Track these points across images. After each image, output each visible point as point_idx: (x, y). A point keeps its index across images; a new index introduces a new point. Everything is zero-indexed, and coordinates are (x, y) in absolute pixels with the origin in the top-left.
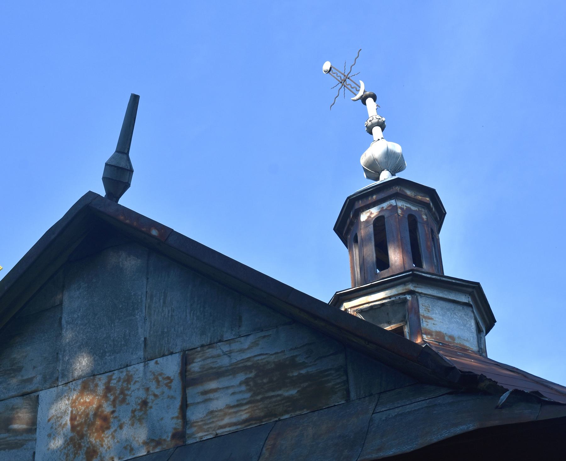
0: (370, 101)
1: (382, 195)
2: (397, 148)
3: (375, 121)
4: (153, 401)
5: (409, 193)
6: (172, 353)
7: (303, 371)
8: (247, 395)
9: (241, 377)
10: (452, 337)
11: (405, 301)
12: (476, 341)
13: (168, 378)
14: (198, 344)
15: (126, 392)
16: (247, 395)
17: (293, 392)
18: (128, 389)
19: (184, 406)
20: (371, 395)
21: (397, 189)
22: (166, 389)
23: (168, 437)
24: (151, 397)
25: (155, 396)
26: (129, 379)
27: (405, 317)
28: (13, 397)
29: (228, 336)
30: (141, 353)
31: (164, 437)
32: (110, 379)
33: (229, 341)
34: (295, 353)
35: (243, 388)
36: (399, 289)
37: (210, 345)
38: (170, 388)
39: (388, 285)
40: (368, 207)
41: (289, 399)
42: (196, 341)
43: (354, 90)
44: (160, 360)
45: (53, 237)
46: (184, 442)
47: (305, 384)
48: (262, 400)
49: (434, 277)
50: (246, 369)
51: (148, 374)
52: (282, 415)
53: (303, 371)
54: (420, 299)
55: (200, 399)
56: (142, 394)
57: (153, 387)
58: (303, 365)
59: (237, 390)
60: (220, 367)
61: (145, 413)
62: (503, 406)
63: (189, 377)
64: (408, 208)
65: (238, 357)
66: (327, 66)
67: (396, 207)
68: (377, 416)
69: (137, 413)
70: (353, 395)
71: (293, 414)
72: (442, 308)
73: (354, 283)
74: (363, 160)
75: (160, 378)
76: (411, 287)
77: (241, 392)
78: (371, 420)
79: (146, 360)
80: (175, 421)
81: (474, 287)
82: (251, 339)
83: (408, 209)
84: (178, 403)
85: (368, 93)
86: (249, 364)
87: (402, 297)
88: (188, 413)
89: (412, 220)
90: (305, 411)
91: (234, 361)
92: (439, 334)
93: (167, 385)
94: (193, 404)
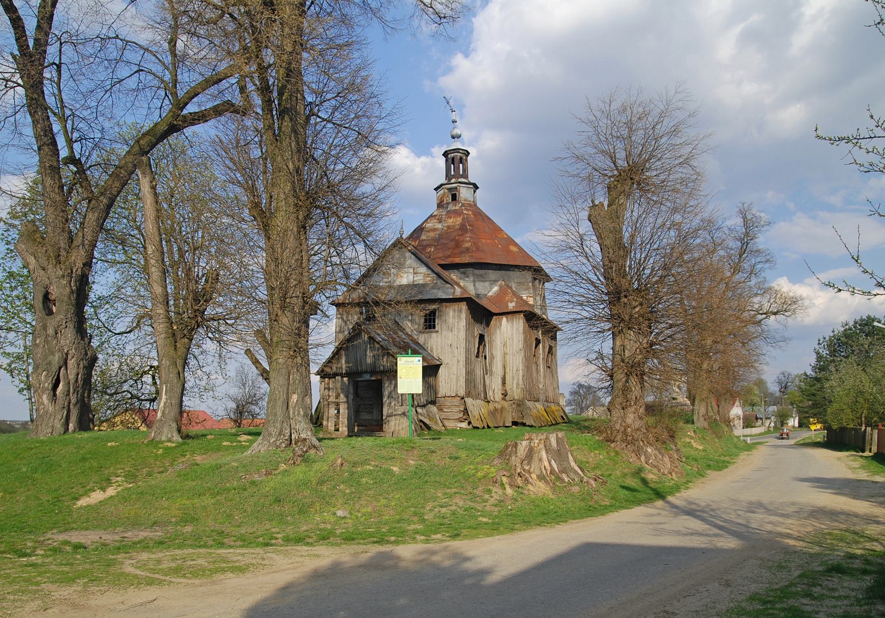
1: (454, 151)
5: (461, 151)
76: (459, 184)
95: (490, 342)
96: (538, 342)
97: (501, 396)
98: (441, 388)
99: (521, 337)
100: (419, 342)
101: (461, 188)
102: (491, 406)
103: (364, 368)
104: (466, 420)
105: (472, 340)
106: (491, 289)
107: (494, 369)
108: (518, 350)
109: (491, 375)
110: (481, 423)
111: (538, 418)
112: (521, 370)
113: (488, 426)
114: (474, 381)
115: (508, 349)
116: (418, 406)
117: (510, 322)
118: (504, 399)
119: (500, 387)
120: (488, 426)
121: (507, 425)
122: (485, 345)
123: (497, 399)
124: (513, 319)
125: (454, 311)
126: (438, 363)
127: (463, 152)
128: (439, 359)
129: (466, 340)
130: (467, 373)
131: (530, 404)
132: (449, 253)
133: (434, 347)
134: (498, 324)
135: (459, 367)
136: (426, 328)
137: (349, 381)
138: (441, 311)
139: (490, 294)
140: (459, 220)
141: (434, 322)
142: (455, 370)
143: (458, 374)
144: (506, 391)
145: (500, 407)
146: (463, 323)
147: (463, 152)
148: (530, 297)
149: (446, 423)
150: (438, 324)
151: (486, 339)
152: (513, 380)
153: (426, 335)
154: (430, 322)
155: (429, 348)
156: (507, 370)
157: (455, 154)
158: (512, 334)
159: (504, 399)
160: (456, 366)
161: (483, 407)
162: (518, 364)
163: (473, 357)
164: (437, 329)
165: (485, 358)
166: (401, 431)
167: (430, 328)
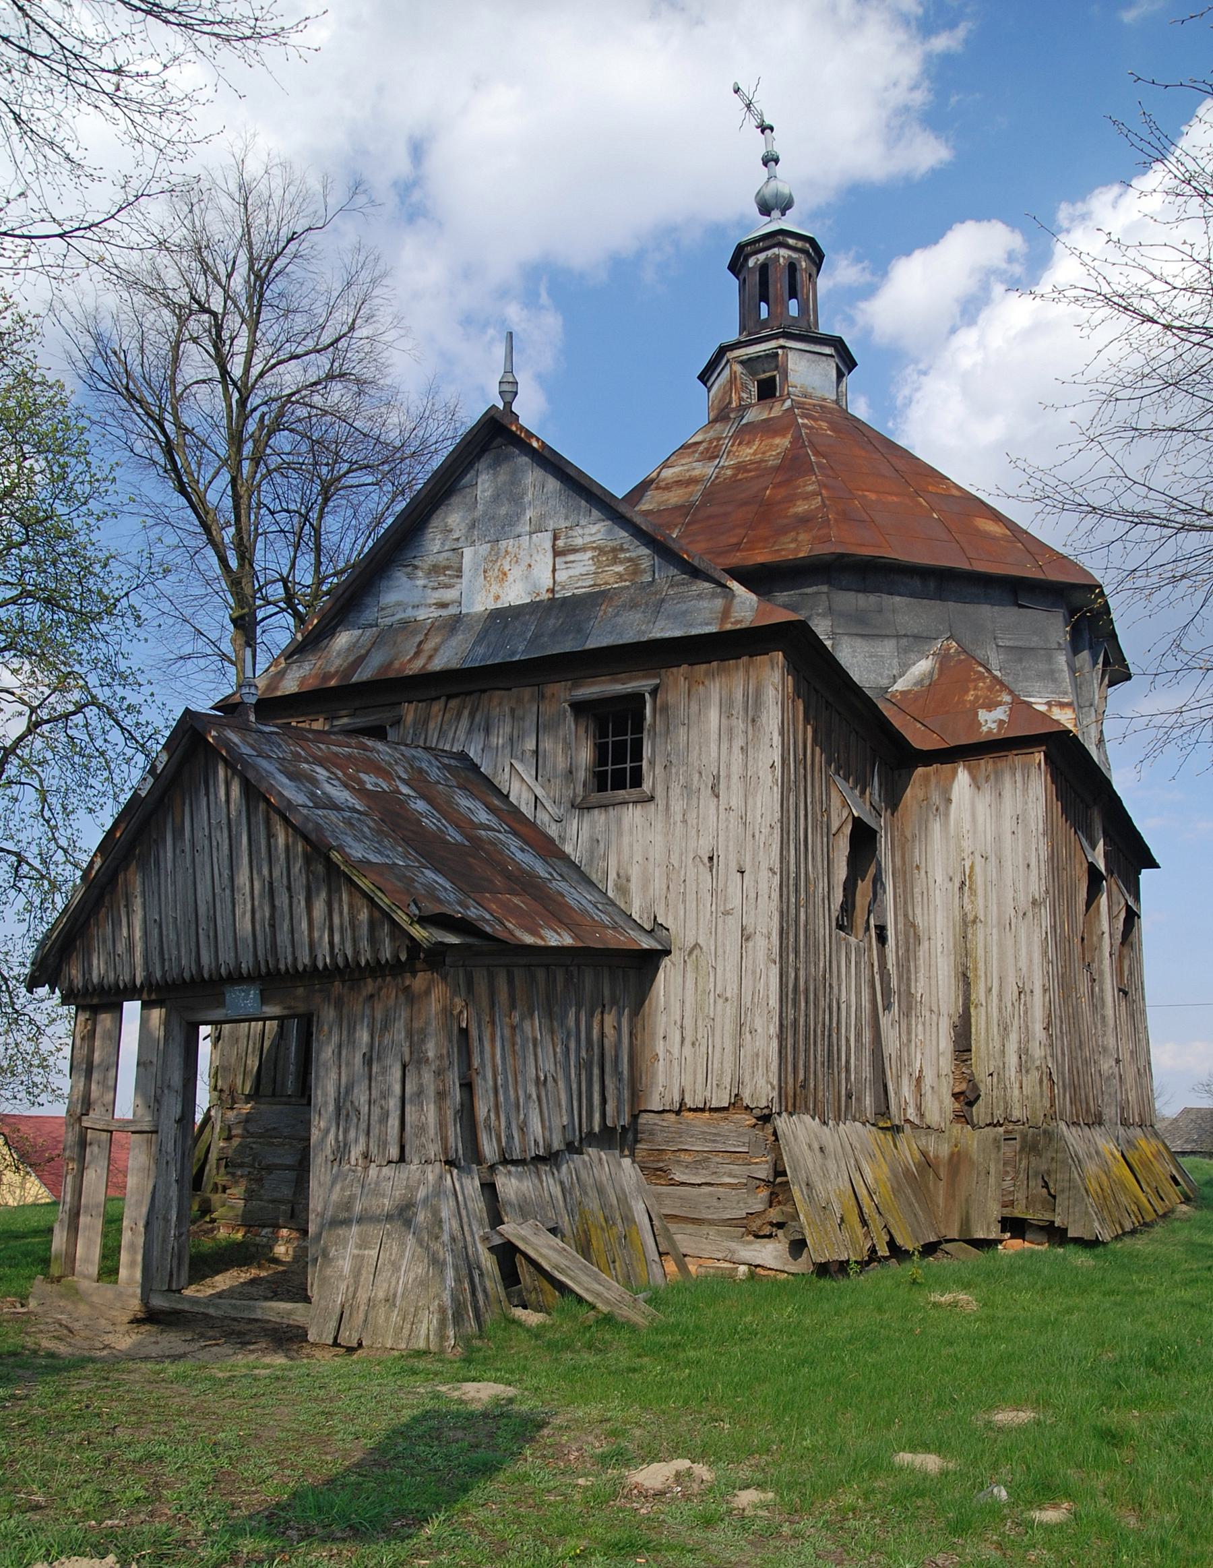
1: (768, 243)
5: (791, 241)
8: (593, 568)
9: (589, 554)
11: (777, 354)
19: (554, 570)
30: (527, 528)
33: (583, 527)
41: (617, 573)
42: (563, 524)
50: (594, 549)
55: (564, 566)
58: (628, 550)
65: (588, 539)
76: (782, 342)
83: (790, 257)
89: (792, 267)
95: (905, 877)
96: (1095, 878)
97: (949, 1104)
98: (661, 1066)
99: (1039, 849)
100: (568, 849)
101: (791, 355)
102: (908, 1150)
103: (226, 957)
104: (780, 1225)
105: (817, 842)
106: (904, 668)
107: (920, 988)
108: (1024, 902)
109: (907, 1012)
110: (860, 1231)
111: (1107, 1202)
112: (1038, 991)
113: (892, 1244)
114: (830, 1033)
115: (980, 901)
116: (505, 1162)
117: (986, 787)
118: (962, 1117)
119: (946, 1063)
120: (892, 1244)
121: (980, 1235)
122: (877, 880)
123: (934, 1116)
124: (998, 775)
125: (726, 709)
126: (646, 943)
127: (800, 244)
128: (657, 928)
129: (784, 832)
130: (790, 993)
131: (1072, 1136)
132: (734, 540)
133: (635, 873)
134: (936, 798)
135: (748, 963)
136: (602, 788)
137: (167, 1023)
138: (665, 708)
139: (900, 686)
140: (783, 442)
141: (638, 755)
142: (732, 976)
143: (747, 999)
144: (971, 1081)
145: (945, 1150)
146: (770, 752)
147: (800, 244)
148: (1062, 705)
149: (685, 1240)
150: (652, 763)
151: (883, 844)
152: (1005, 1029)
153: (599, 817)
154: (619, 758)
155: (612, 876)
156: (979, 993)
157: (770, 253)
158: (998, 839)
159: (962, 1117)
160: (734, 959)
161: (872, 1156)
162: (1023, 963)
163: (823, 927)
164: (646, 786)
165: (882, 938)
166: (382, 1311)
167: (619, 785)
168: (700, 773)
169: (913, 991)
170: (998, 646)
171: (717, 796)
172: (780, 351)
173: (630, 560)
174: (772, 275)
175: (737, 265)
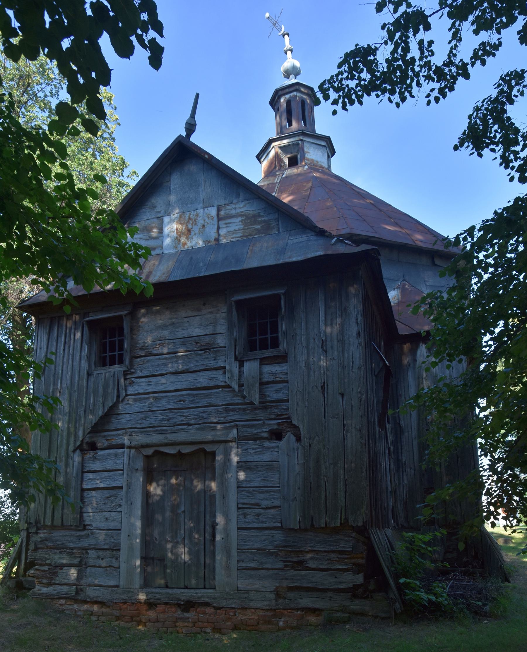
0: (286, 36)
2: (297, 64)
3: (288, 48)
4: (207, 225)
6: (213, 206)
7: (263, 219)
8: (242, 226)
9: (240, 219)
10: (317, 162)
11: (298, 144)
12: (327, 163)
13: (212, 216)
14: (223, 203)
15: (197, 221)
16: (242, 226)
17: (259, 227)
18: (197, 219)
19: (218, 228)
20: (287, 231)
21: (297, 87)
22: (211, 221)
23: (213, 240)
24: (206, 224)
25: (207, 223)
26: (197, 215)
27: (298, 151)
28: (154, 218)
29: (235, 201)
30: (202, 205)
31: (211, 240)
32: (190, 214)
34: (260, 211)
35: (241, 223)
36: (297, 138)
37: (228, 204)
38: (213, 220)
39: (291, 136)
40: (284, 94)
41: (257, 229)
42: (223, 202)
43: (279, 30)
44: (209, 208)
45: (167, 153)
46: (219, 242)
47: (263, 224)
48: (248, 229)
49: (311, 133)
50: (242, 216)
51: (205, 214)
52: (255, 235)
53: (263, 219)
54: (305, 144)
55: (225, 226)
56: (202, 222)
57: (207, 219)
58: (263, 216)
59: (238, 224)
60: (232, 214)
61: (204, 230)
62: (333, 244)
63: (220, 217)
64: (301, 97)
65: (238, 211)
66: (267, 15)
67: (296, 96)
68: (289, 241)
69: (201, 230)
70: (281, 230)
71: (259, 235)
72: (314, 148)
73: (277, 134)
74: (282, 69)
75: (209, 216)
76: (301, 138)
77: (240, 225)
78: (287, 243)
79: (204, 208)
80: (215, 234)
81: (327, 138)
82: (243, 204)
84: (216, 227)
85: (285, 32)
86: (242, 214)
87: (297, 142)
88: (220, 231)
89: (303, 102)
90: (263, 235)
91: (237, 212)
92: (312, 160)
93: (212, 219)
94: (222, 228)
101: (306, 145)
141: (275, 329)
157: (292, 94)
164: (283, 346)
168: (314, 339)
169: (400, 458)
170: (426, 285)
171: (326, 351)
172: (300, 142)
173: (264, 221)
174: (293, 104)
175: (274, 103)
